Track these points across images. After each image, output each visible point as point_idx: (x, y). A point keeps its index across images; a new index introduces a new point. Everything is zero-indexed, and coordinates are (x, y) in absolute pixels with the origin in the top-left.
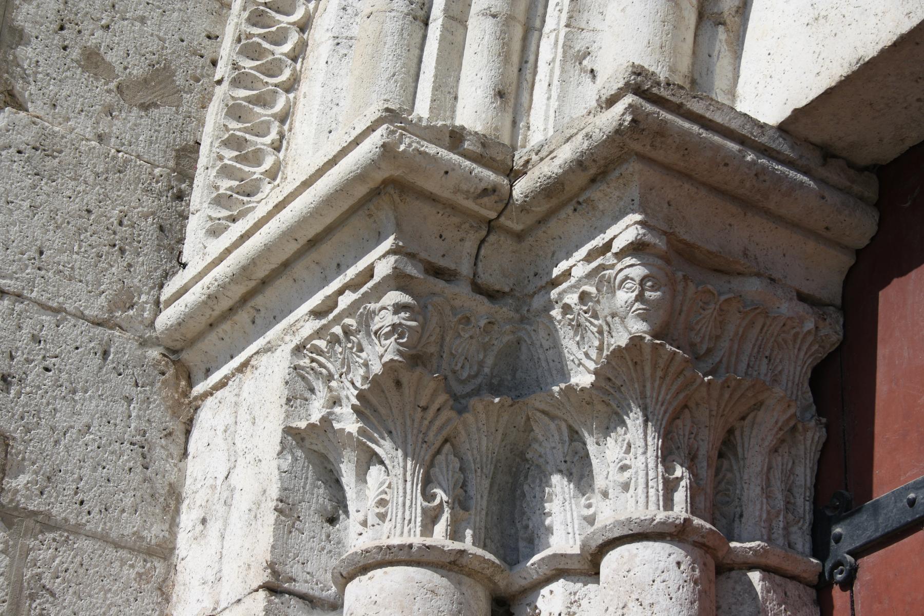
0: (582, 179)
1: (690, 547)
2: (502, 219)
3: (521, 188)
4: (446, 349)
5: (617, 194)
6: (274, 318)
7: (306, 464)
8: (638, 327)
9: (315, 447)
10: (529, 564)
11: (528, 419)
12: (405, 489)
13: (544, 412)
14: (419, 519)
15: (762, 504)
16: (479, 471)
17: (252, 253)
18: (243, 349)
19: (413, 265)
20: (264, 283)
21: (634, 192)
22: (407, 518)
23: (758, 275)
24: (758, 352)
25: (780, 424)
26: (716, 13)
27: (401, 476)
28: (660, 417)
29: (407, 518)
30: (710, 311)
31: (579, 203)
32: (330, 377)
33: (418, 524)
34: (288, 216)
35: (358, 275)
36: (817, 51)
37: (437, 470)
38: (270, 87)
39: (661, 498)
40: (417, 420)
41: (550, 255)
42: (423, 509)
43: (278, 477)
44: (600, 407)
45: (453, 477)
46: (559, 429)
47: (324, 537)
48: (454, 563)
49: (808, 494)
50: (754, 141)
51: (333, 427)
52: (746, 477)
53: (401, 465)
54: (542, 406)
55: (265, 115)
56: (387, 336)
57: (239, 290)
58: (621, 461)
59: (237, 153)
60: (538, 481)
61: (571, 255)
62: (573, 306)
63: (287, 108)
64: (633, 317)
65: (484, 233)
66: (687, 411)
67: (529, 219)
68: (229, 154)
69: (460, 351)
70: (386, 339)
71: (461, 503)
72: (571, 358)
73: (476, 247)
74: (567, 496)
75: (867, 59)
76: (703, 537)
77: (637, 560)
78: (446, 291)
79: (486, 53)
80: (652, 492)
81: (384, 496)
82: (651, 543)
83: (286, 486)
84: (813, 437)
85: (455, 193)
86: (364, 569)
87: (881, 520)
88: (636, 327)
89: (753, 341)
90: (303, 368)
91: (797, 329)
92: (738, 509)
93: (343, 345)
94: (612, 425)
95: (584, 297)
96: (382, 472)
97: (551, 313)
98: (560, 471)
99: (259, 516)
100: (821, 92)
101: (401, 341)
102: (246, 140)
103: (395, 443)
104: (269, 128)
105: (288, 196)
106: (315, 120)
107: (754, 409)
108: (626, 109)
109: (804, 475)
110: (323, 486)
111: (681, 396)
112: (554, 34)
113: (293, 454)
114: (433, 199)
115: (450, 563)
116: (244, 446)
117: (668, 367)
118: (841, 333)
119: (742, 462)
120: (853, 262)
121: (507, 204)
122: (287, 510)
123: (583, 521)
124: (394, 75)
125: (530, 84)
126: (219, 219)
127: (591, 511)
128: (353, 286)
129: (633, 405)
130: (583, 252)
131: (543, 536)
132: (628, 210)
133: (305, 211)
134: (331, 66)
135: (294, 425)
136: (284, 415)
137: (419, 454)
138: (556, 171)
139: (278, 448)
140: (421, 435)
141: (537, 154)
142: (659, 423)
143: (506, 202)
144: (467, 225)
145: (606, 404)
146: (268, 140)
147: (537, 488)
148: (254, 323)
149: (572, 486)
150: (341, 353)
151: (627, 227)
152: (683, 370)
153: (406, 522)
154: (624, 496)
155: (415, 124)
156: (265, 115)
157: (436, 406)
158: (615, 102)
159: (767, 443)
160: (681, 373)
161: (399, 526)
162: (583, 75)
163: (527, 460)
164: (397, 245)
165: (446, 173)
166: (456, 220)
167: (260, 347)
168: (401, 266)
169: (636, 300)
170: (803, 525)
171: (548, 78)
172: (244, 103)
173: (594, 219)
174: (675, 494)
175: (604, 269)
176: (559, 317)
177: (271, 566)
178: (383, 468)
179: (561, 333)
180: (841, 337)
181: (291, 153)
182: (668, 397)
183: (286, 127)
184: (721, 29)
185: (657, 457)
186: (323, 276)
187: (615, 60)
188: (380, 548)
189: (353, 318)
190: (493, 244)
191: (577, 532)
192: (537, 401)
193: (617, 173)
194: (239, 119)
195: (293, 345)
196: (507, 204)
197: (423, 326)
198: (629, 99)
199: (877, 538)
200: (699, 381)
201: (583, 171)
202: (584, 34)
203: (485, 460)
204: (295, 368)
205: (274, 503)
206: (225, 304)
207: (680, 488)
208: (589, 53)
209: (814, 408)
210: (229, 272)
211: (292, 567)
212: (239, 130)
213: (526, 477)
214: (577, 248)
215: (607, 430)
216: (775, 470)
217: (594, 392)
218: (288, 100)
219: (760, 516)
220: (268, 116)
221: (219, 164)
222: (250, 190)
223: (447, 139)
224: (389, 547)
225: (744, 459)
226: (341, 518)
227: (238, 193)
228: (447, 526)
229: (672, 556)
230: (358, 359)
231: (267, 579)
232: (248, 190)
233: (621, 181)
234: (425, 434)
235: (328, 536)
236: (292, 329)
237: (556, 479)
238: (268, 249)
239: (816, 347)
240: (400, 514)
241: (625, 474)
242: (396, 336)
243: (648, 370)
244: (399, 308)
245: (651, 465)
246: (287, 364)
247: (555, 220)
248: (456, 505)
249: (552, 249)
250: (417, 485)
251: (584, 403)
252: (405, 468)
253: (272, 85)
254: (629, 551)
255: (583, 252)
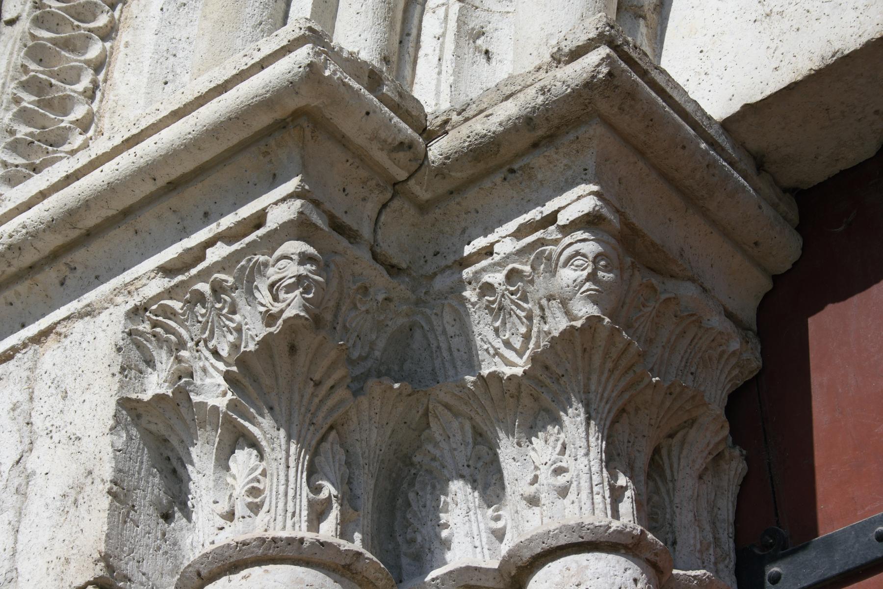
0: (529, 138)
1: (645, 565)
2: (412, 182)
3: (437, 150)
4: (340, 320)
5: (565, 162)
6: (97, 277)
7: (141, 446)
8: (584, 310)
9: (153, 427)
10: (428, 578)
11: (426, 413)
12: (287, 476)
13: (447, 406)
14: (305, 513)
15: (695, 533)
16: (366, 467)
17: (87, 193)
18: (43, 315)
19: (318, 214)
20: (89, 235)
21: (589, 160)
22: (290, 509)
23: (692, 280)
24: (685, 366)
25: (711, 446)
26: (636, 6)
27: (283, 461)
28: (604, 415)
29: (290, 509)
30: (649, 309)
31: (512, 171)
32: (181, 344)
33: (304, 518)
34: (148, 149)
35: (239, 223)
36: (773, 46)
37: (323, 459)
38: (82, 31)
39: (609, 507)
40: (307, 397)
41: (459, 232)
42: (309, 501)
43: (112, 455)
44: (526, 400)
45: (339, 469)
46: (462, 428)
47: (159, 535)
48: (347, 567)
49: (731, 530)
50: (704, 130)
51: (190, 400)
52: (677, 500)
53: (284, 447)
54: (448, 399)
55: (76, 61)
56: (289, 289)
57: (56, 241)
58: (555, 463)
59: (37, 98)
60: (429, 487)
61: (492, 231)
62: (496, 285)
63: (103, 56)
64: (581, 299)
65: (389, 195)
66: (625, 415)
67: (441, 187)
68: (28, 100)
69: (354, 325)
70: (287, 293)
71: (349, 499)
72: (485, 347)
73: (377, 211)
74: (471, 505)
75: (846, 52)
76: (656, 555)
77: (589, 573)
78: (348, 252)
79: (370, 14)
80: (598, 499)
81: (256, 484)
82: (604, 555)
83: (120, 466)
84: (735, 468)
85: (371, 140)
86: (234, 567)
87: (837, 557)
88: (584, 310)
89: (682, 352)
90: (141, 334)
91: (724, 347)
92: (670, 535)
93: (209, 305)
94: (540, 424)
95: (513, 276)
96: (253, 457)
97: (464, 294)
98: (462, 477)
99: (81, 501)
100: (783, 87)
101: (306, 296)
102: (51, 85)
103: (276, 421)
104: (79, 76)
105: (147, 128)
106: (146, 69)
107: (684, 427)
108: (603, 59)
109: (727, 509)
110: (158, 475)
111: (627, 396)
112: (444, 8)
113: (128, 432)
114: (343, 141)
115: (344, 566)
116: (48, 425)
117: (619, 358)
118: (761, 360)
119: (671, 485)
120: (770, 287)
121: (421, 165)
122: (120, 495)
123: (491, 535)
124: (260, 24)
125: (412, 58)
126: (17, 166)
127: (500, 525)
128: (228, 237)
129: (573, 399)
130: (512, 226)
131: (437, 551)
132: (579, 180)
133: (177, 143)
134: (167, 14)
135: (134, 396)
136: (118, 385)
137: (305, 437)
138: (493, 129)
139: (111, 422)
140: (309, 415)
141: (459, 114)
142: (602, 423)
143: (420, 162)
144: (374, 182)
145: (532, 403)
146: (79, 87)
147: (429, 496)
148: (62, 284)
149: (476, 494)
150: (203, 316)
151: (579, 198)
152: (633, 365)
153: (289, 515)
154: (560, 502)
155: (337, 52)
156: (76, 61)
157: (330, 382)
158: (580, 56)
159: (697, 466)
160: (630, 368)
161: (280, 519)
162: (477, 54)
163: (412, 464)
164: (303, 187)
165: (368, 113)
166: (363, 173)
167: (72, 310)
168: (307, 212)
169: (588, 279)
170: (729, 563)
171: (437, 52)
172: (49, 45)
173: (527, 190)
174: (620, 505)
175: (543, 245)
176: (474, 299)
177: (105, 558)
178: (255, 452)
179: (475, 317)
180: (760, 364)
181: (109, 104)
182: (614, 394)
183: (101, 77)
184: (642, 22)
185: (601, 460)
186: (180, 227)
187: (542, 29)
188: (262, 540)
189: (229, 274)
190: (395, 211)
191: (486, 547)
192: (443, 393)
193: (571, 136)
194: (40, 62)
195: (129, 306)
196: (421, 165)
197: (327, 281)
198: (604, 51)
199: (834, 577)
200: (646, 381)
201: (529, 131)
202: (478, 12)
203: (372, 456)
204: (130, 334)
205: (108, 485)
206: (29, 258)
207: (625, 499)
208: (484, 34)
209: (730, 439)
210: (47, 216)
211: (127, 564)
212: (43, 73)
213: (412, 484)
214: (500, 223)
215: (531, 430)
216: (707, 501)
217: (526, 382)
218: (104, 49)
219: (695, 545)
220: (80, 61)
221: (15, 109)
222: (57, 139)
223: (366, 78)
224: (274, 540)
225: (673, 480)
226: (176, 515)
227: (39, 141)
228: (337, 524)
229: (628, 572)
230: (227, 323)
231: (101, 573)
232: (52, 139)
233: (574, 146)
234: (314, 415)
235: (164, 535)
236: (128, 289)
237: (456, 486)
238: (112, 189)
239: (736, 372)
240: (281, 505)
241: (559, 476)
242: (301, 290)
243: (597, 360)
244: (305, 259)
245: (595, 468)
246: (121, 327)
247: (477, 189)
248: (346, 502)
249: (463, 224)
250: (302, 473)
251: (507, 395)
252: (288, 451)
253: (85, 29)
254: (577, 562)
255: (512, 226)
